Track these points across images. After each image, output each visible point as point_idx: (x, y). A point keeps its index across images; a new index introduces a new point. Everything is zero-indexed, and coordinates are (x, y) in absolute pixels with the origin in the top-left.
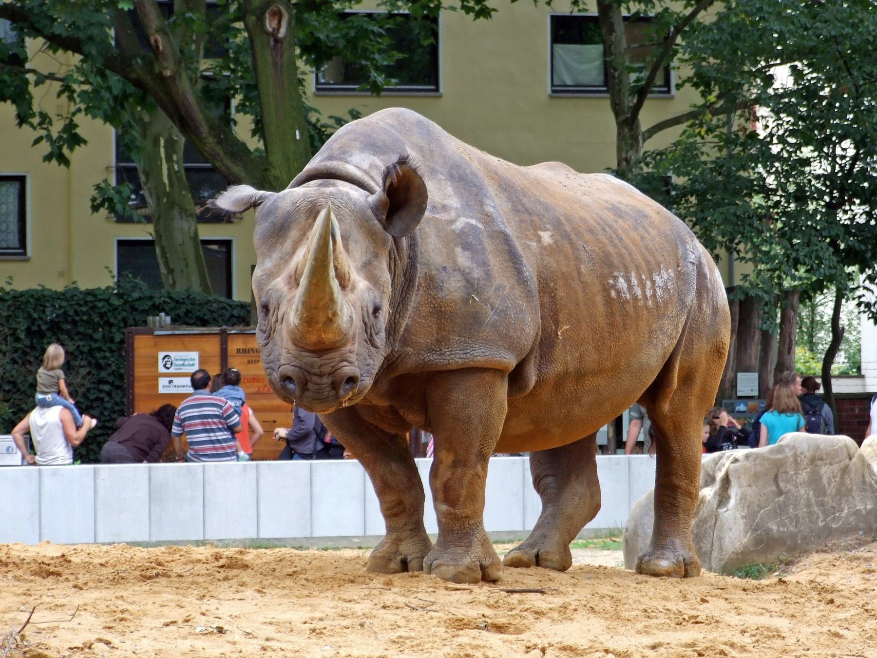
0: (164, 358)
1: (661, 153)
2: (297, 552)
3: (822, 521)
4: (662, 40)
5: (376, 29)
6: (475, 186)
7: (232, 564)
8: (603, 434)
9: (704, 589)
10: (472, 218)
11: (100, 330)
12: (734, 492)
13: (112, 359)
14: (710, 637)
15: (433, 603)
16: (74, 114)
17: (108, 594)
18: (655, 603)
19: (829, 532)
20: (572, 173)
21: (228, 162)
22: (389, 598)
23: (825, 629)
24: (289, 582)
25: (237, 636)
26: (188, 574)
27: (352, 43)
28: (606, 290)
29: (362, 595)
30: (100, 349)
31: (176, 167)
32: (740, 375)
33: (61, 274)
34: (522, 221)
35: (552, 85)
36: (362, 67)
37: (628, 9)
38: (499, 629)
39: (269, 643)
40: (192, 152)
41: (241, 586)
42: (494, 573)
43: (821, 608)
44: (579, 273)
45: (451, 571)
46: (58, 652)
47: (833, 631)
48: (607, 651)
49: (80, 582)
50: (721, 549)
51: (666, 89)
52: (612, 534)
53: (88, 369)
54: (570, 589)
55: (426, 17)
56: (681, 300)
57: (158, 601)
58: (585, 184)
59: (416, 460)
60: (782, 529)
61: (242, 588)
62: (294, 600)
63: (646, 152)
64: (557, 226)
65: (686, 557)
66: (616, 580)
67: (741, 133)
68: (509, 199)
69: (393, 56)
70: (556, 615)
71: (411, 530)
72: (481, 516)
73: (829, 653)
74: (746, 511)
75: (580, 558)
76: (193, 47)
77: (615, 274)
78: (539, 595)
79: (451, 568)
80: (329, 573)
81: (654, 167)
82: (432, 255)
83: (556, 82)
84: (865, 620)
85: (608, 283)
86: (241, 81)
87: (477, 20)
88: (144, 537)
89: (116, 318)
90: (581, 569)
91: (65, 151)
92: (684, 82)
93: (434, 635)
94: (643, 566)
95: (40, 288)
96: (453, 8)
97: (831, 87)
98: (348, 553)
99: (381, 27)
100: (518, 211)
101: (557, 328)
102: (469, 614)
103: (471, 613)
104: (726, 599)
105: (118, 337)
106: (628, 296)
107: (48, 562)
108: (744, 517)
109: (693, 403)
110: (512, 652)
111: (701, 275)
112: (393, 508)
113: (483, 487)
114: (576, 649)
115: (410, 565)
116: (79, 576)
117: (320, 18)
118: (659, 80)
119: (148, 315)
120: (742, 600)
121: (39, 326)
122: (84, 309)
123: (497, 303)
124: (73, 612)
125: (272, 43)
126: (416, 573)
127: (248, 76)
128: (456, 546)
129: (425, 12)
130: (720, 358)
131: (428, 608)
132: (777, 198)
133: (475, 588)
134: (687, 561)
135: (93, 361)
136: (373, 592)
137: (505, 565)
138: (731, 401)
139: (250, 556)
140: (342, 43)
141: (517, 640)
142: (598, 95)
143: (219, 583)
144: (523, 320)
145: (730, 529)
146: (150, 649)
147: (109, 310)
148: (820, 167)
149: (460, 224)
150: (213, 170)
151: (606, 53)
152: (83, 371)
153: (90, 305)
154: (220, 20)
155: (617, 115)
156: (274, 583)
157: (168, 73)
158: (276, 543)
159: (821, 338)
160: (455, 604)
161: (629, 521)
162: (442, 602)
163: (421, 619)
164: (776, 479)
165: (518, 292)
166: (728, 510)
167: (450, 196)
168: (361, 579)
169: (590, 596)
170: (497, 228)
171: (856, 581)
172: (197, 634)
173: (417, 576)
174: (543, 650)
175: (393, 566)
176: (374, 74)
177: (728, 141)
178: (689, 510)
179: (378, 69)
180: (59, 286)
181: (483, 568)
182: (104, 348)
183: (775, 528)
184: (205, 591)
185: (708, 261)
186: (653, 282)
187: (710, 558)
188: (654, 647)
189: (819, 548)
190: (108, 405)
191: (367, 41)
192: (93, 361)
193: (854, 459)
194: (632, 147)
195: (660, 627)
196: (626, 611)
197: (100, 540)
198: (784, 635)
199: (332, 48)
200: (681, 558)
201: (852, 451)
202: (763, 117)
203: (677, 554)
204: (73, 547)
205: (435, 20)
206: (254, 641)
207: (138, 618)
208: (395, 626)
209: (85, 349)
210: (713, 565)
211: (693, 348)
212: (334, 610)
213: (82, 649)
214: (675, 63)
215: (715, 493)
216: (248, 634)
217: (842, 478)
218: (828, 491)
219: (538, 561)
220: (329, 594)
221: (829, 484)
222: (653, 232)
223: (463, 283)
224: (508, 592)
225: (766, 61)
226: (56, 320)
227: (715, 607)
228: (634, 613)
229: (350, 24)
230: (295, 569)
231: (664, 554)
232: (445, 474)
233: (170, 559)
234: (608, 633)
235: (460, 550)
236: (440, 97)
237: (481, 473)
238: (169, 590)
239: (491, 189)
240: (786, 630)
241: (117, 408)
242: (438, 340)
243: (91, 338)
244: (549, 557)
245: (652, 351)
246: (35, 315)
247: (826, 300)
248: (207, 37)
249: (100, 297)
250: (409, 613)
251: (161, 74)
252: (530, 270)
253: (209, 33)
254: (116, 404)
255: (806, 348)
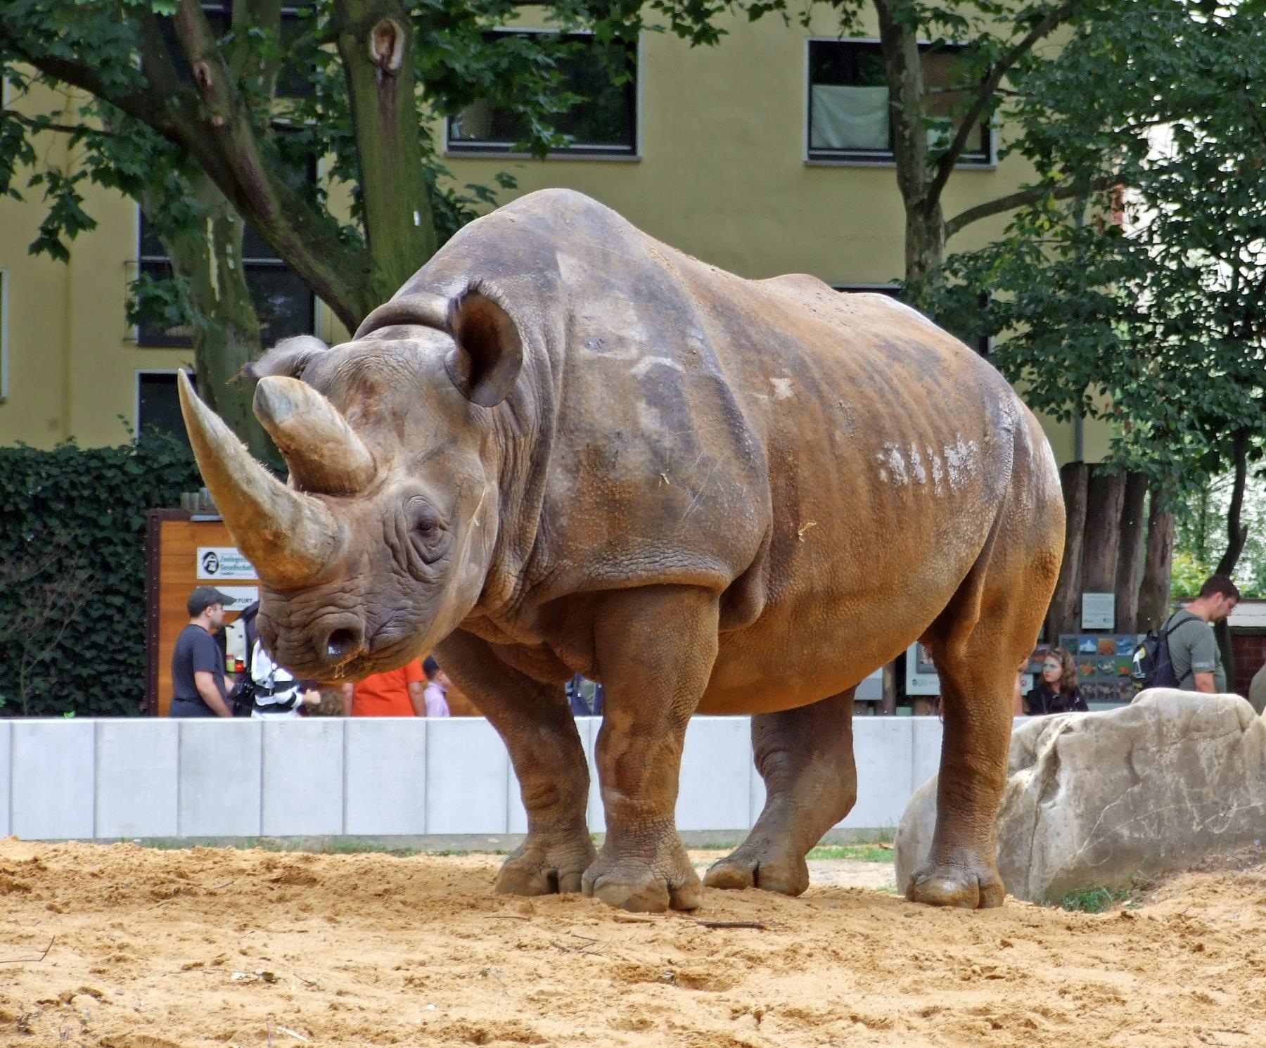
0: (206, 557)
1: (974, 257)
2: (395, 860)
3: (1198, 824)
4: (978, 82)
5: (541, 58)
6: (674, 308)
7: (292, 877)
8: (874, 683)
9: (1006, 926)
10: (666, 356)
11: (109, 511)
12: (1065, 777)
13: (127, 557)
14: (1013, 1000)
15: (594, 942)
16: (76, 179)
17: (101, 920)
18: (932, 947)
19: (1208, 841)
20: (828, 292)
21: (308, 257)
22: (527, 932)
23: (1187, 990)
24: (377, 906)
25: (293, 988)
26: (223, 891)
27: (504, 78)
28: (872, 468)
29: (487, 927)
30: (109, 541)
31: (231, 264)
32: (1086, 596)
33: (53, 424)
34: (746, 362)
35: (810, 148)
36: (520, 116)
37: (929, 36)
38: (693, 982)
39: (341, 999)
40: (256, 241)
41: (304, 910)
42: (689, 899)
43: (1184, 958)
44: (833, 442)
45: (623, 893)
46: (21, 1008)
47: (1199, 992)
48: (855, 1019)
49: (58, 902)
50: (1043, 864)
51: (983, 157)
52: (883, 836)
53: (90, 572)
54: (804, 924)
55: (618, 41)
56: (988, 486)
57: (176, 930)
58: (846, 309)
59: (577, 719)
60: (1136, 835)
61: (305, 915)
62: (383, 934)
63: (952, 256)
64: (800, 370)
65: (982, 875)
66: (875, 910)
67: (1096, 229)
68: (728, 328)
69: (568, 99)
70: (779, 963)
71: (565, 830)
72: (671, 811)
73: (1191, 1026)
74: (1082, 806)
75: (833, 874)
76: (261, 80)
77: (887, 445)
78: (755, 932)
79: (623, 888)
80: (438, 893)
81: (966, 277)
82: (597, 416)
83: (815, 143)
84: (1249, 978)
85: (876, 459)
86: (332, 132)
87: (697, 47)
88: (167, 830)
89: (133, 494)
90: (824, 892)
91: (63, 237)
92: (1011, 147)
93: (594, 991)
94: (917, 890)
95: (17, 446)
96: (659, 29)
97: (1235, 158)
98: (472, 862)
99: (549, 56)
100: (741, 346)
101: (797, 525)
102: (648, 959)
103: (652, 957)
104: (1040, 942)
105: (136, 523)
106: (906, 480)
107: (11, 870)
108: (1078, 816)
109: (1004, 644)
110: (711, 1018)
111: (1020, 450)
112: (540, 795)
113: (676, 768)
114: (808, 1015)
115: (562, 884)
116: (57, 892)
117: (456, 40)
118: (973, 141)
119: (183, 490)
120: (1065, 944)
121: (15, 505)
122: (85, 479)
123: (703, 486)
124: (45, 946)
125: (380, 77)
126: (570, 895)
127: (343, 123)
128: (632, 855)
129: (617, 33)
130: (1047, 577)
131: (586, 949)
132: (1149, 328)
133: (660, 920)
134: (984, 883)
135: (98, 559)
136: (504, 923)
137: (707, 885)
138: (1072, 636)
139: (322, 865)
140: (488, 77)
141: (719, 1000)
142: (880, 163)
143: (271, 906)
144: (742, 512)
145: (1058, 834)
146: (161, 1005)
147: (123, 482)
148: (1220, 277)
149: (642, 368)
150: (286, 269)
151: (894, 95)
152: (82, 575)
153: (95, 474)
154: (302, 41)
155: (907, 196)
156: (354, 906)
157: (220, 121)
158: (371, 842)
159: (1215, 540)
160: (627, 944)
161: (904, 819)
162: (607, 939)
163: (575, 966)
164: (1129, 760)
165: (735, 469)
166: (1054, 805)
167: (630, 324)
168: (487, 904)
169: (832, 935)
170: (706, 372)
171: (1247, 918)
172: (233, 984)
173: (572, 900)
174: (758, 1016)
175: (535, 883)
176: (536, 126)
177: (1077, 239)
178: (991, 807)
179: (542, 118)
180: (47, 444)
181: (672, 889)
182: (115, 540)
183: (1126, 833)
184: (248, 918)
185: (1032, 430)
186: (945, 459)
187: (1027, 877)
188: (926, 1014)
189: (1193, 866)
190: (120, 627)
191: (527, 75)
192: (98, 559)
193: (1248, 731)
194: (929, 244)
195: (938, 983)
196: (886, 958)
197: (104, 833)
198: (1124, 998)
199: (472, 85)
200: (975, 879)
201: (1246, 718)
202: (1129, 204)
203: (968, 872)
204: (52, 847)
205: (632, 46)
206: (319, 995)
207: (145, 958)
208: (535, 976)
209: (86, 541)
210: (1031, 888)
211: (1005, 561)
212: (443, 950)
213: (58, 1004)
214: (997, 118)
215: (1036, 779)
216: (311, 984)
217: (1230, 758)
218: (1208, 779)
219: (757, 879)
220: (437, 925)
221: (1210, 766)
222: (947, 384)
223: (649, 456)
224: (708, 926)
225: (1137, 117)
226: (42, 496)
227: (1023, 954)
228: (899, 961)
229: (501, 49)
230: (387, 886)
231: (948, 872)
232: (620, 745)
233: (198, 867)
234: (858, 991)
235: (637, 862)
236: (638, 162)
237: (673, 746)
238: (193, 915)
239: (700, 313)
240: (1129, 991)
241: (133, 632)
242: (610, 543)
243: (95, 524)
244: (774, 875)
245: (941, 563)
246: (10, 488)
247: (1225, 482)
248: (282, 65)
249: (110, 462)
250: (557, 956)
251: (208, 121)
252: (756, 433)
253: (284, 60)
254: (133, 625)
255: (1194, 556)
